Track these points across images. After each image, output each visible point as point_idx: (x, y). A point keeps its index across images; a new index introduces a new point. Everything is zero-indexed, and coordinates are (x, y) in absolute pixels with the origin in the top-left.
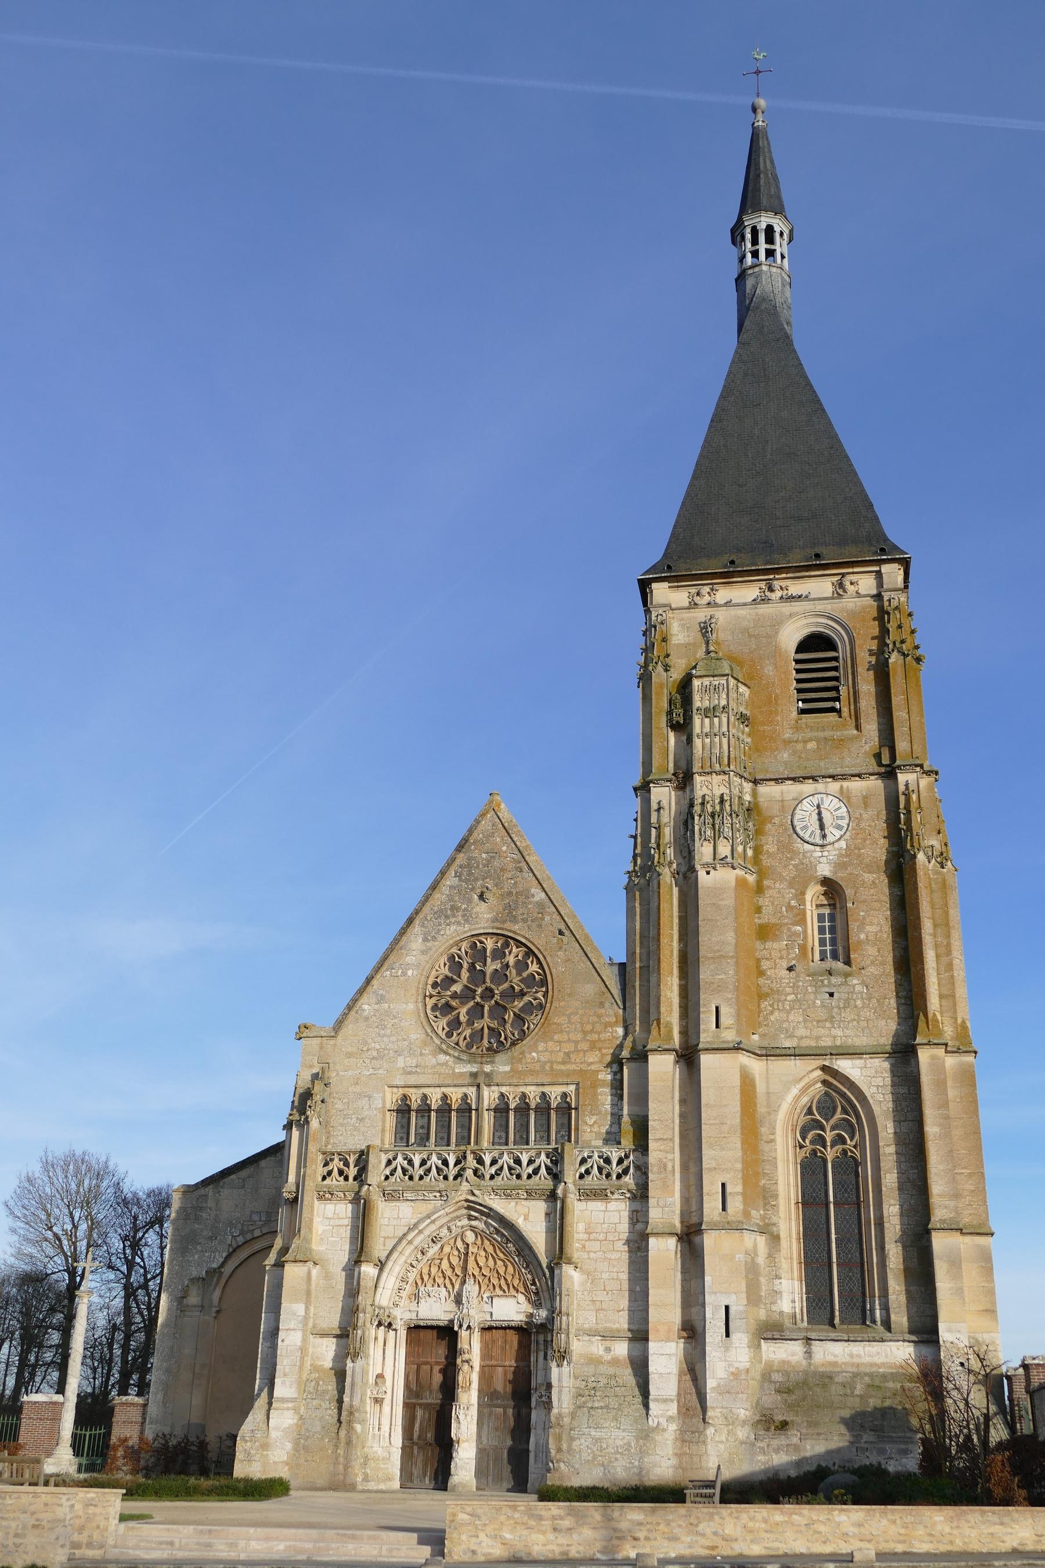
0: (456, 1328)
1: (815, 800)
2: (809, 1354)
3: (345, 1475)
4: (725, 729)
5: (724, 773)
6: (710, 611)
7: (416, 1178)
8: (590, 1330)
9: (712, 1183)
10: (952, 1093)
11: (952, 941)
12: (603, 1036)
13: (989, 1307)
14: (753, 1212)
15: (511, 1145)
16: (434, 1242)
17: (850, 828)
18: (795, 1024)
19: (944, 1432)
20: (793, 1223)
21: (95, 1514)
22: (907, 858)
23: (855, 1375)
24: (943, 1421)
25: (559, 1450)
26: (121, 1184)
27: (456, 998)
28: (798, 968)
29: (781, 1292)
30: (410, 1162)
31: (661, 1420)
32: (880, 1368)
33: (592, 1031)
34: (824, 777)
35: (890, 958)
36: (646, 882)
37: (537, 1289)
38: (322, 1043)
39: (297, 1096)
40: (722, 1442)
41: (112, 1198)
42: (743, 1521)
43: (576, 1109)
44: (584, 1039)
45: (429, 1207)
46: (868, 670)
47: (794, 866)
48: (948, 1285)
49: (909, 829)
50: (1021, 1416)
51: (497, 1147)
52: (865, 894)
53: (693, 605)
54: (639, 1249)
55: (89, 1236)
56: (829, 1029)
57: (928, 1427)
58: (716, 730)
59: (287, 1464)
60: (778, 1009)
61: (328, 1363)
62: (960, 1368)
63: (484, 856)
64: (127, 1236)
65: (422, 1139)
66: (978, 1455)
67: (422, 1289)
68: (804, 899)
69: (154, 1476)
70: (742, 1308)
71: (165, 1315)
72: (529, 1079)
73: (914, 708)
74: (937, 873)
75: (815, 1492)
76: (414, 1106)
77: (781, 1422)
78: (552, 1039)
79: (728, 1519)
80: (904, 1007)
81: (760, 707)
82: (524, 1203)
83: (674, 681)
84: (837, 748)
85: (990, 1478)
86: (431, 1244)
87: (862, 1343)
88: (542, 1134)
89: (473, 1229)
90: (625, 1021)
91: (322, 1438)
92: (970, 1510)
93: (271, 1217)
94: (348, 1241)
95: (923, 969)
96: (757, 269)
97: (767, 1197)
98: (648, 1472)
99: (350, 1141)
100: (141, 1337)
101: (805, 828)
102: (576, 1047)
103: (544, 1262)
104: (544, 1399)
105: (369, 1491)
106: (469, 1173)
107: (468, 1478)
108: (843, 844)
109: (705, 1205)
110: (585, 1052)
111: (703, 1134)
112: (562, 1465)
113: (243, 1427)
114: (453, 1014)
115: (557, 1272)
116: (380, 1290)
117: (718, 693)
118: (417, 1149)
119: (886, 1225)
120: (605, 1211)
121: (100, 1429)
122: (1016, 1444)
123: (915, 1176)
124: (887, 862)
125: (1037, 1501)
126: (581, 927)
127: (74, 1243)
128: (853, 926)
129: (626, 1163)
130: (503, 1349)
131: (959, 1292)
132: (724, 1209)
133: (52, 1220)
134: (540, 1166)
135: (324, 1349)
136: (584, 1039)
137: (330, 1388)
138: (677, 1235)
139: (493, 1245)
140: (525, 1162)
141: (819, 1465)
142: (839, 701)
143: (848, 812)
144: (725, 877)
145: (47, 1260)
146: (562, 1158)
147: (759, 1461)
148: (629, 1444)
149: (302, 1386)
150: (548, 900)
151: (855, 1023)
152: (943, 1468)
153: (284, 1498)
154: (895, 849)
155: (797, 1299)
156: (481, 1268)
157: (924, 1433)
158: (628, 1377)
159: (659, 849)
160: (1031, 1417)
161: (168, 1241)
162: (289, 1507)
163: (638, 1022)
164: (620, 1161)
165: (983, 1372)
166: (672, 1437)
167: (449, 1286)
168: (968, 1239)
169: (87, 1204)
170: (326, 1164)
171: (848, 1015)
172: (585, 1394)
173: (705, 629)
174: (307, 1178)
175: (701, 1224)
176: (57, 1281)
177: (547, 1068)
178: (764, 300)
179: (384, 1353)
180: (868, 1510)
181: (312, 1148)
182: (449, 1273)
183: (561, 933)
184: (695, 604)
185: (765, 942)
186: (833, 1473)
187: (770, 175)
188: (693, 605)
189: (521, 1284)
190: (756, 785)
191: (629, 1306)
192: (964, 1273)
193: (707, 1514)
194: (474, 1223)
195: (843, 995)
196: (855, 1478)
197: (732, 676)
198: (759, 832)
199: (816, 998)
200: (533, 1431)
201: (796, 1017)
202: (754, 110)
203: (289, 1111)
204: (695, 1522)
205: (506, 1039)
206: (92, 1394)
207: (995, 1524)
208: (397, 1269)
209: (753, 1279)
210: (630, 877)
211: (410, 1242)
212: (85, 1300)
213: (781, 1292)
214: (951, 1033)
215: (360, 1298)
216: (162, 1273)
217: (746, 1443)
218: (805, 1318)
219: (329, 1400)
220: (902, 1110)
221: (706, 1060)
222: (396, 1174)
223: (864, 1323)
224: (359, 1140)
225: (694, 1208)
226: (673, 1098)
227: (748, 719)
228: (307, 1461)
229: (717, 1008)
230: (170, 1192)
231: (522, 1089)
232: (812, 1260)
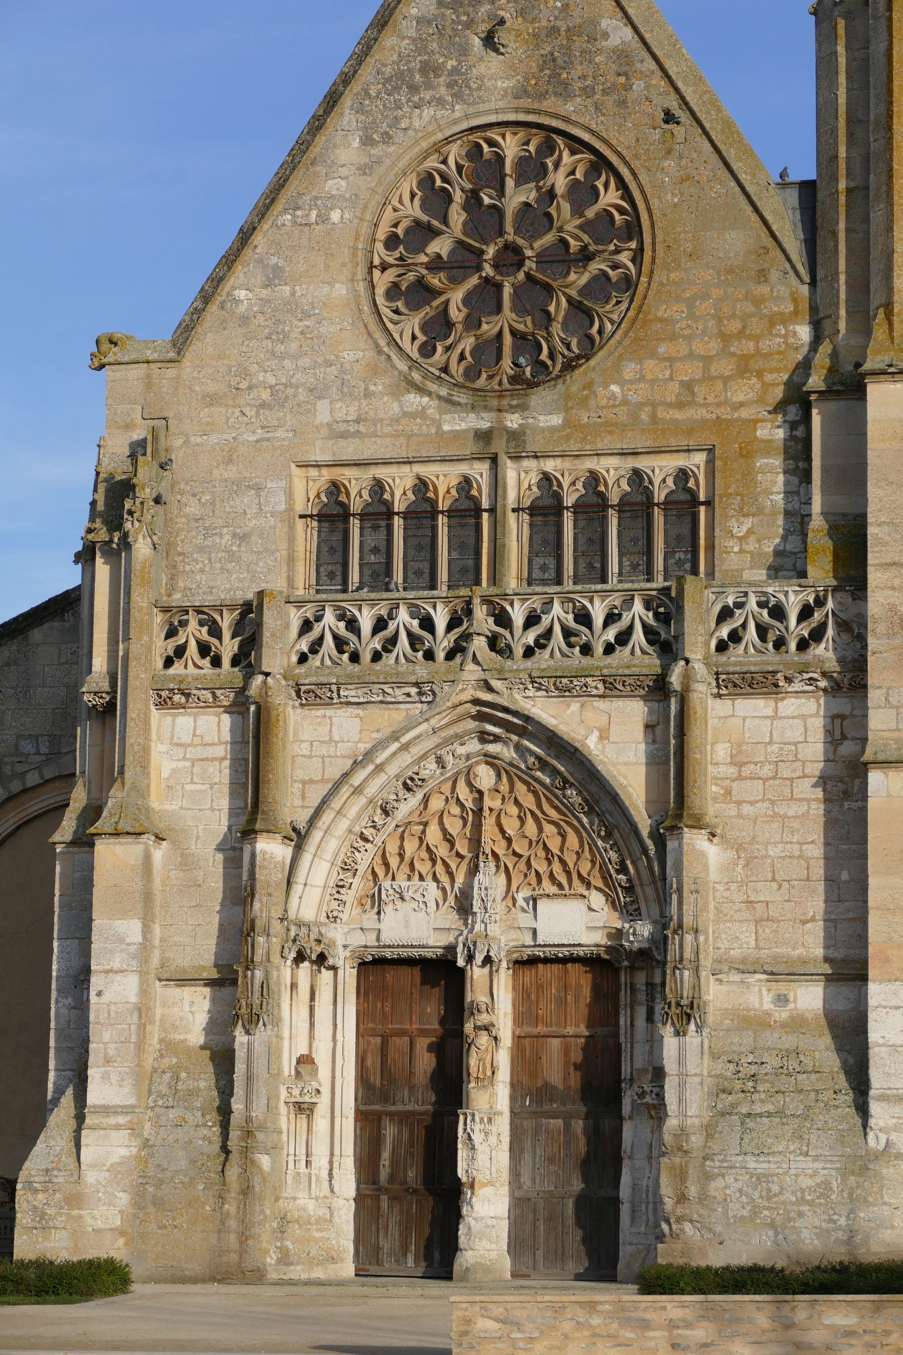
0: (461, 963)
3: (241, 1253)
7: (366, 657)
8: (744, 961)
12: (765, 345)
15: (568, 585)
25: (682, 1198)
27: (440, 269)
30: (352, 625)
38: (148, 376)
44: (724, 351)
45: (395, 716)
54: (846, 794)
59: (122, 1233)
65: (375, 575)
67: (387, 884)
78: (653, 354)
86: (402, 793)
88: (636, 558)
89: (491, 760)
90: (814, 309)
91: (192, 1183)
94: (226, 790)
102: (706, 369)
103: (644, 824)
104: (648, 1099)
105: (292, 1283)
106: (479, 644)
107: (493, 1255)
110: (726, 380)
112: (688, 1227)
113: (27, 1164)
114: (435, 303)
115: (671, 845)
116: (297, 889)
120: (773, 718)
126: (714, 103)
129: (817, 616)
130: (562, 1002)
134: (631, 627)
135: (187, 1008)
136: (724, 351)
137: (202, 1084)
139: (535, 793)
140: (598, 618)
146: (680, 609)
148: (826, 1184)
150: (640, 45)
153: (120, 1298)
156: (509, 840)
163: (843, 312)
164: (806, 613)
167: (444, 879)
170: (171, 633)
174: (132, 664)
181: (140, 600)
182: (442, 851)
183: (669, 118)
191: (826, 912)
194: (492, 748)
200: (626, 1163)
205: (551, 356)
208: (332, 845)
215: (257, 905)
219: (202, 1108)
222: (324, 650)
224: (241, 581)
228: (162, 1227)
231: (591, 464)
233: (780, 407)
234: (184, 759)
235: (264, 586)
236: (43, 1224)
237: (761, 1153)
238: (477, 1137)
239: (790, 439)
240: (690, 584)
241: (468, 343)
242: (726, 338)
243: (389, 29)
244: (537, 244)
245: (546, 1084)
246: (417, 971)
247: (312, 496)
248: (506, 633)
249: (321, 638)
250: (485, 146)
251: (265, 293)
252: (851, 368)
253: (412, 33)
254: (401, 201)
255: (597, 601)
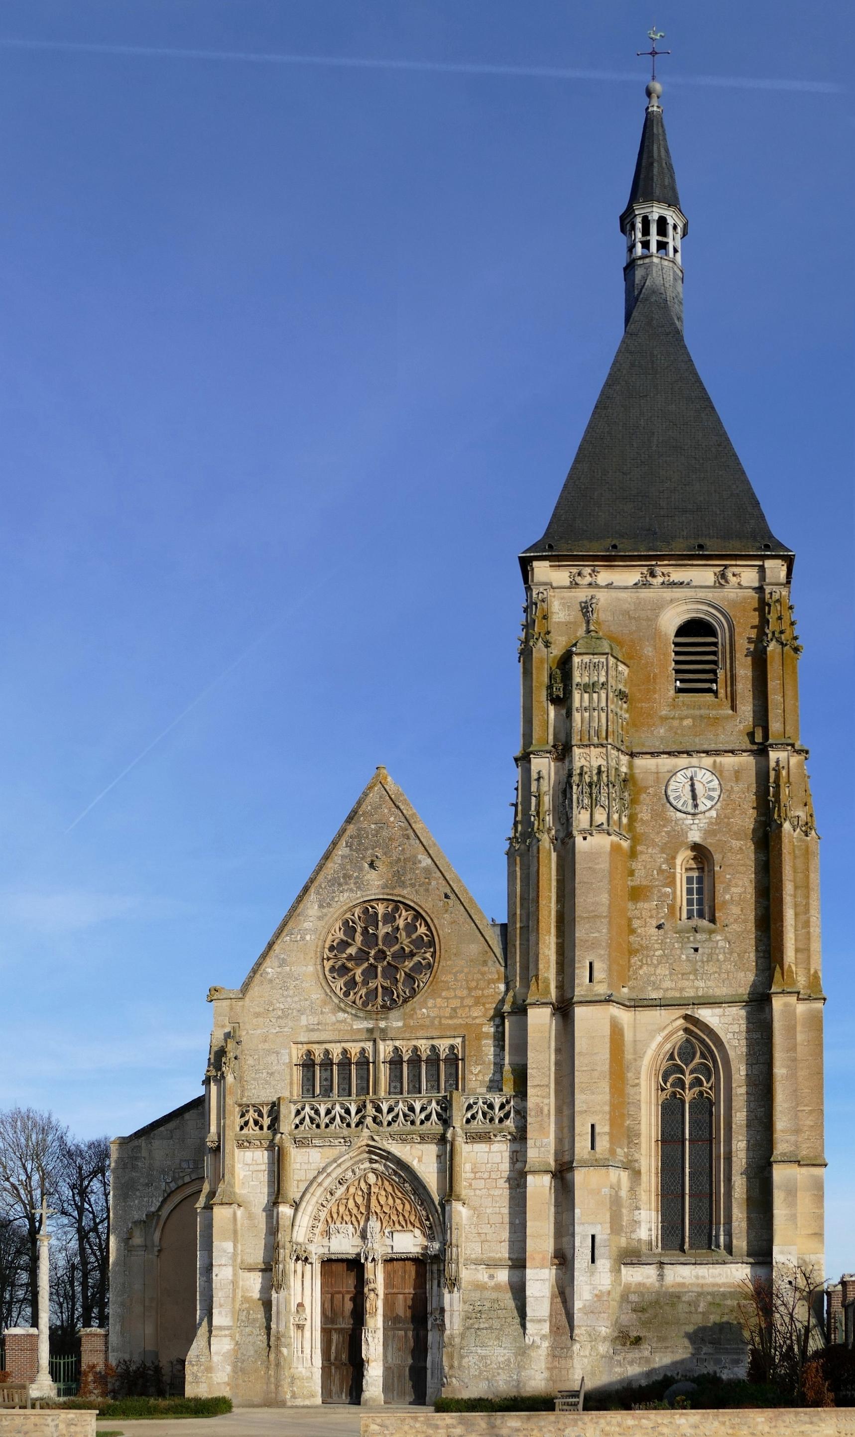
0: (363, 1261)
1: (689, 773)
2: (661, 1276)
3: (277, 1393)
4: (603, 704)
5: (602, 746)
6: (591, 592)
7: (323, 1126)
8: (476, 1259)
9: (583, 1125)
10: (800, 1037)
11: (811, 902)
12: (486, 992)
13: (817, 1230)
14: (619, 1150)
15: (405, 1095)
16: (341, 1184)
17: (721, 799)
18: (662, 977)
19: (771, 1343)
20: (653, 1159)
21: (76, 1433)
22: (774, 826)
23: (700, 1294)
24: (771, 1334)
25: (451, 1367)
26: (64, 1138)
27: (352, 960)
28: (666, 927)
29: (639, 1222)
30: (317, 1112)
31: (536, 1338)
32: (720, 1287)
33: (476, 988)
34: (698, 752)
35: (752, 917)
36: (526, 848)
37: (430, 1224)
38: (231, 1005)
39: (213, 1053)
40: (585, 1357)
41: (58, 1151)
42: (601, 1426)
43: (463, 1059)
44: (469, 995)
45: (334, 1152)
46: (746, 656)
47: (667, 832)
48: (784, 1212)
49: (778, 800)
50: (836, 1328)
51: (393, 1096)
52: (731, 858)
53: (574, 585)
54: (518, 1185)
55: (42, 1186)
56: (693, 981)
57: (757, 1339)
58: (595, 705)
59: (228, 1385)
60: (647, 964)
61: (256, 1295)
62: (788, 1286)
63: (373, 826)
64: (74, 1184)
65: (326, 1090)
66: (797, 1363)
67: (332, 1226)
68: (675, 863)
69: (120, 1398)
70: (606, 1237)
71: (114, 1254)
72: (420, 1034)
73: (789, 693)
74: (801, 840)
75: (661, 1399)
76: (318, 1061)
77: (635, 1338)
78: (440, 996)
79: (589, 1424)
80: (762, 960)
81: (639, 686)
82: (418, 1146)
83: (555, 657)
84: (712, 725)
85: (806, 1383)
86: (338, 1185)
87: (707, 1266)
88: (433, 1083)
89: (374, 1171)
90: (506, 977)
91: (256, 1361)
92: (787, 1412)
93: (198, 1165)
94: (266, 1184)
95: (782, 926)
96: (647, 261)
97: (631, 1136)
98: (524, 1386)
99: (263, 1094)
100: (97, 1274)
101: (678, 798)
102: (462, 1003)
103: (436, 1199)
104: (438, 1322)
105: (297, 1407)
106: (369, 1120)
107: (377, 1393)
108: (713, 813)
109: (576, 1145)
110: (470, 1007)
111: (576, 1081)
112: (454, 1380)
113: (189, 1353)
114: (350, 974)
115: (447, 1208)
116: (296, 1228)
117: (598, 670)
118: (322, 1099)
119: (734, 1159)
120: (488, 1152)
121: (72, 1358)
122: (830, 1352)
123: (762, 1114)
124: (754, 830)
125: (842, 1402)
126: (465, 890)
127: (30, 1192)
128: (719, 888)
129: (507, 1108)
130: (403, 1278)
131: (793, 1218)
132: (593, 1148)
133: (8, 1172)
134: (431, 1113)
135: (252, 1282)
136: (469, 995)
137: (259, 1316)
138: (551, 1172)
139: (392, 1185)
140: (418, 1109)
141: (665, 1376)
142: (716, 683)
143: (720, 784)
144: (601, 842)
145: (8, 1208)
146: (451, 1105)
147: (616, 1373)
148: (509, 1360)
149: (236, 1315)
150: (434, 866)
151: (716, 975)
152: (767, 1375)
153: (228, 1415)
154: (763, 819)
155: (653, 1228)
156: (382, 1206)
157: (754, 1345)
158: (508, 1300)
159: (538, 816)
160: (844, 1329)
161: (111, 1188)
162: (233, 1422)
163: (518, 979)
164: (502, 1107)
165: (807, 1290)
166: (545, 1353)
167: (356, 1223)
168: (804, 1170)
169: (36, 1157)
170: (242, 1116)
171: (711, 968)
172: (473, 1316)
173: (586, 609)
174: (227, 1129)
175: (572, 1162)
176: (20, 1227)
177: (436, 1022)
178: (654, 292)
179: (303, 1285)
180: (704, 1413)
181: (230, 1101)
182: (355, 1211)
183: (447, 896)
184: (577, 584)
185: (637, 902)
186: (677, 1381)
187: (664, 165)
188: (574, 585)
189: (417, 1220)
190: (632, 758)
191: (510, 1237)
192: (798, 1201)
193: (572, 1420)
194: (375, 1166)
195: (707, 950)
196: (694, 1385)
197: (612, 656)
198: (634, 801)
199: (682, 953)
200: (429, 1350)
201: (663, 970)
202: (649, 93)
203: (206, 1068)
204: (562, 1427)
205: (398, 997)
206: (61, 1327)
207: (806, 1423)
208: (310, 1208)
209: (616, 1211)
210: (511, 844)
211: (320, 1184)
212: (46, 1243)
213: (639, 1222)
214: (803, 983)
215: (280, 1235)
216: (108, 1217)
217: (606, 1357)
218: (660, 1245)
219: (259, 1327)
220: (755, 1054)
221: (580, 1012)
222: (305, 1123)
223: (710, 1248)
224: (271, 1093)
225: (566, 1147)
226: (549, 1048)
227: (627, 696)
228: (244, 1381)
229: (591, 964)
230: (108, 1144)
231: (414, 1043)
232: (668, 1192)
233: (492, 1019)
234: (249, 1170)
235: (280, 1095)
236: (197, 1381)
237: (483, 1346)
238: (370, 1339)
239: (496, 1032)
240: (455, 1094)
241: (363, 991)
242: (470, 989)
243: (329, 860)
244: (392, 950)
245: (397, 1315)
246: (345, 1264)
247: (300, 1056)
248: (380, 1115)
249: (304, 1118)
250: (370, 908)
251: (279, 970)
252: (521, 1002)
253: (339, 862)
254: (335, 932)
255: (417, 1102)
